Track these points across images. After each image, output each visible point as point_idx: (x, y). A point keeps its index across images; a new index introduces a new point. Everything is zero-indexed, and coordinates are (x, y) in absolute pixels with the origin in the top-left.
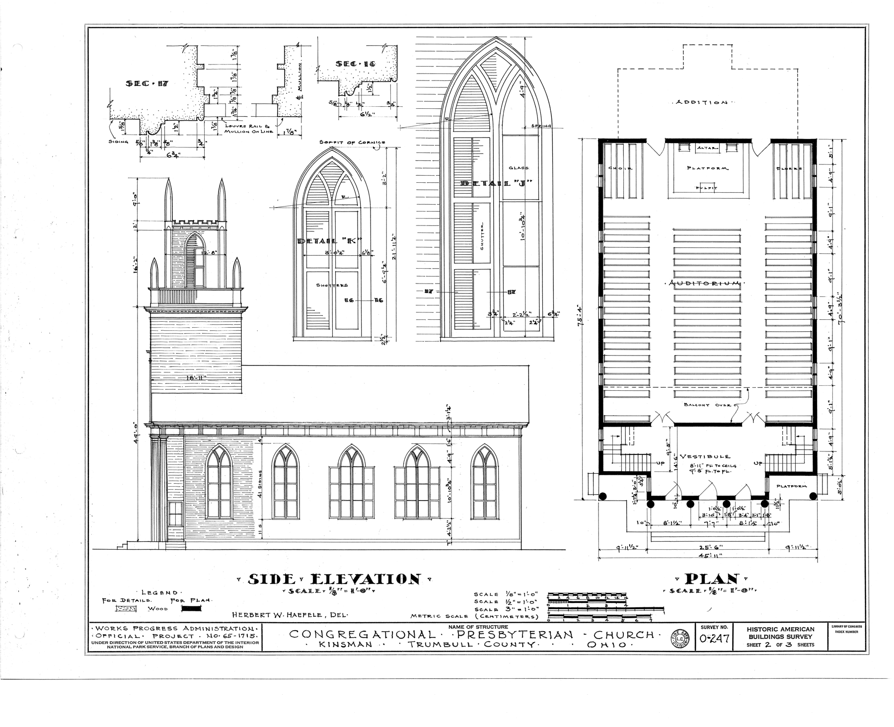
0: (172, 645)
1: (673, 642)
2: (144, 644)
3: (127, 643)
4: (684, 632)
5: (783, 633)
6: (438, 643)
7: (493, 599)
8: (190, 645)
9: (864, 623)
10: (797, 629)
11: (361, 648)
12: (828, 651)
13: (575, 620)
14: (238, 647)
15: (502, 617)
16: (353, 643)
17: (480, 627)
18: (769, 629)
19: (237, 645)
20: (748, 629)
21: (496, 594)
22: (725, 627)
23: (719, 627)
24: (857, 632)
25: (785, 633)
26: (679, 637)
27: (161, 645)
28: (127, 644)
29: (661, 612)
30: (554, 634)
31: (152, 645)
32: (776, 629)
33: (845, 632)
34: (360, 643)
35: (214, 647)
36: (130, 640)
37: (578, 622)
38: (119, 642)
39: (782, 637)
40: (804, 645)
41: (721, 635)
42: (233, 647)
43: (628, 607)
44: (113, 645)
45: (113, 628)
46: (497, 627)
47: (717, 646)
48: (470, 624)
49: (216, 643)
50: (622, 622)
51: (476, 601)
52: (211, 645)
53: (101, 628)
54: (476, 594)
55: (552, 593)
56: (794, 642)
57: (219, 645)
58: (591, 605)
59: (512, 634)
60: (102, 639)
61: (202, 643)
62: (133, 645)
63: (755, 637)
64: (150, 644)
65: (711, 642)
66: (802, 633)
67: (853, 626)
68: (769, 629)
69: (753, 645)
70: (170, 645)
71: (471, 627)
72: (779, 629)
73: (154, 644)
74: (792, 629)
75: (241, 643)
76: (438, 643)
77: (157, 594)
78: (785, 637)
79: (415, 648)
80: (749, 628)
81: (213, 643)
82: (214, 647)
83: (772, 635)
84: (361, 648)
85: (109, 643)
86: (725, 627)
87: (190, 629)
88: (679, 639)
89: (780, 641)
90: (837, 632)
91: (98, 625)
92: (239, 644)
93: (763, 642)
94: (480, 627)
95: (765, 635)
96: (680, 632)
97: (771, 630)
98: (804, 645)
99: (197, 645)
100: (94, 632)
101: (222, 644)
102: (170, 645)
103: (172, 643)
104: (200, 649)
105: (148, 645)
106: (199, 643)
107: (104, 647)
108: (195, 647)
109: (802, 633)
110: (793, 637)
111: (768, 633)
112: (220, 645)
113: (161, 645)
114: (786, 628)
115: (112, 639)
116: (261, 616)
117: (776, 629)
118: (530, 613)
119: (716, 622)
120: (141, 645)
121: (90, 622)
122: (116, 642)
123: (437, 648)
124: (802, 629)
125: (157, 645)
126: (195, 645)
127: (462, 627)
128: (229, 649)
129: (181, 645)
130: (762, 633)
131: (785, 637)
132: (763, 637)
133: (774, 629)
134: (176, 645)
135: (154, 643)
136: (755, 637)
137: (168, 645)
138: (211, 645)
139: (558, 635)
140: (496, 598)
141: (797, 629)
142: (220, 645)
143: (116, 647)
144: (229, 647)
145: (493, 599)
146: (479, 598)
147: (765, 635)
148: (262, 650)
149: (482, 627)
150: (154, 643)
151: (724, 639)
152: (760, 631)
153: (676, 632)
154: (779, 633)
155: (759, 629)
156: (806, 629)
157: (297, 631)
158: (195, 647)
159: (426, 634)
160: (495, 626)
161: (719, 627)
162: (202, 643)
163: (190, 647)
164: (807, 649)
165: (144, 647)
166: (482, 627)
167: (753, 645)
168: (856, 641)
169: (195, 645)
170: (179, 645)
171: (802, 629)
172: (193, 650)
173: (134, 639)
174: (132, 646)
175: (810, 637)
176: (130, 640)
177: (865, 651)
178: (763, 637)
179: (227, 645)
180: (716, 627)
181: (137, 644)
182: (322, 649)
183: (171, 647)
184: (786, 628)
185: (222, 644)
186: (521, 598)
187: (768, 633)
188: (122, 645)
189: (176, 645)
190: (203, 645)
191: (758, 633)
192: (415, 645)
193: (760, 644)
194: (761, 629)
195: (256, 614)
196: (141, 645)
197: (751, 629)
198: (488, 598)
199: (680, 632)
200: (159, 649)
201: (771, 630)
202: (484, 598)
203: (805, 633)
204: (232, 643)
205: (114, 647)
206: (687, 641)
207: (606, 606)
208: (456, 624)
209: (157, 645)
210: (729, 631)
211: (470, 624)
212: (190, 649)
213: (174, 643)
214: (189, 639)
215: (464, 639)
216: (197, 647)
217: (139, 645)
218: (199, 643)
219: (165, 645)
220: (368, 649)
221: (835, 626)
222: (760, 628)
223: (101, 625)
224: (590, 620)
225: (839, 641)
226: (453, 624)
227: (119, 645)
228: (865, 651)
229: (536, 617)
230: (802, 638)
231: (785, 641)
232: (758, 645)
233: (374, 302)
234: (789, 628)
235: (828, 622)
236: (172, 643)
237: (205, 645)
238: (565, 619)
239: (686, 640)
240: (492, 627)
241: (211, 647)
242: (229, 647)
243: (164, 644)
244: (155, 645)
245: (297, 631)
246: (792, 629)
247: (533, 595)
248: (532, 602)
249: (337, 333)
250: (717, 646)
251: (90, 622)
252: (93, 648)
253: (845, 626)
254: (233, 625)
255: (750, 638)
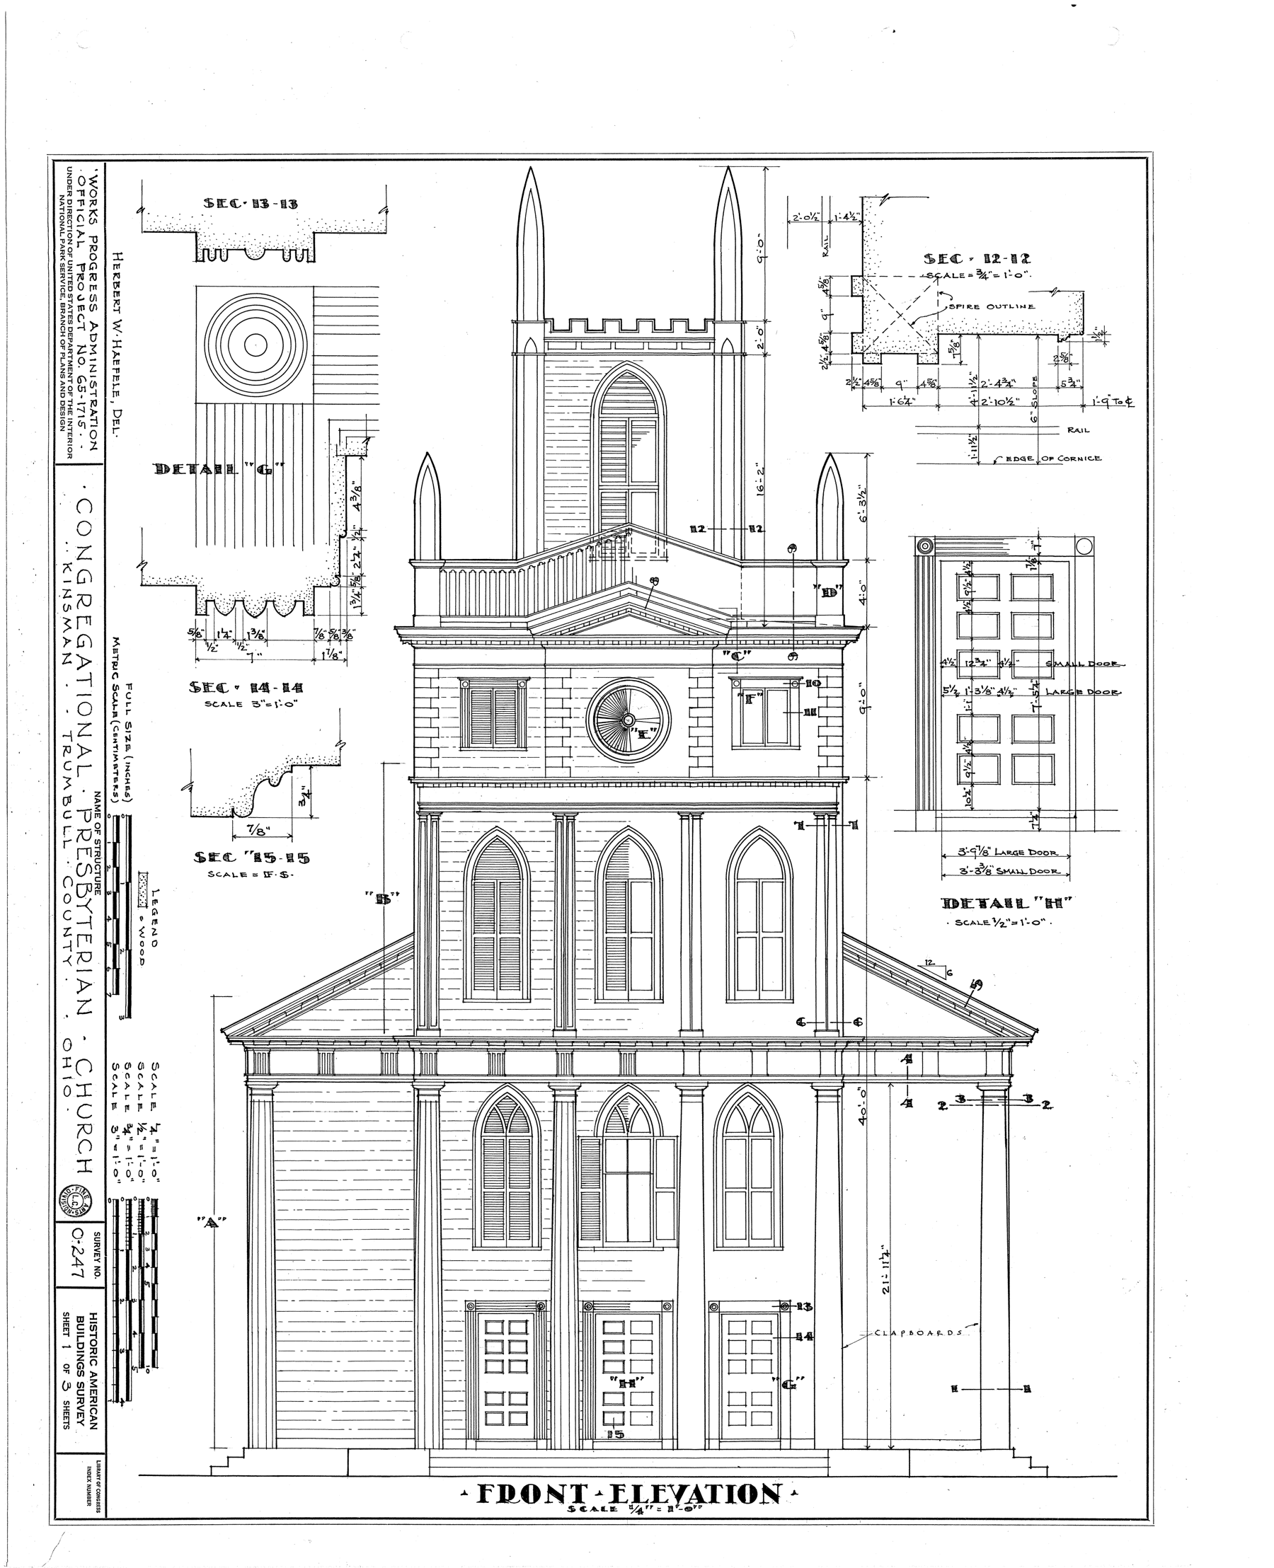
0: (67, 307)
1: (70, 1188)
2: (67, 258)
3: (70, 229)
4: (87, 1208)
5: (87, 1374)
6: (70, 785)
7: (146, 1101)
8: (66, 338)
9: (104, 1517)
10: (94, 1400)
11: (60, 642)
12: (56, 1453)
13: (110, 913)
14: (62, 423)
15: (116, 753)
16: (70, 628)
17: (98, 846)
18: (94, 1350)
19: (66, 420)
20: (93, 1314)
21: (154, 1104)
22: (97, 1274)
23: (97, 1264)
24: (89, 1504)
25: (86, 1380)
26: (79, 1199)
27: (66, 288)
28: (66, 229)
29: (123, 1012)
30: (85, 977)
31: (66, 272)
32: (94, 1363)
33: (89, 1483)
34: (70, 641)
35: (63, 380)
36: (75, 234)
37: (106, 969)
38: (70, 216)
39: (81, 1373)
40: (67, 1412)
41: (83, 1264)
42: (62, 414)
43: (133, 1336)
44: (66, 205)
45: (94, 202)
46: (98, 875)
47: (65, 1258)
48: (102, 829)
49: (70, 384)
50: (106, 944)
51: (141, 1066)
52: (67, 375)
53: (94, 184)
54: (155, 1066)
55: (156, 1215)
56: (72, 1396)
57: (66, 389)
58: (135, 1275)
59: (86, 906)
60: (76, 186)
61: (70, 359)
62: (66, 239)
63: (80, 1327)
64: (67, 269)
65: (73, 1247)
66: (87, 1408)
67: (98, 1496)
68: (94, 1350)
69: (66, 1323)
70: (67, 303)
71: (98, 831)
72: (94, 1369)
73: (67, 276)
74: (94, 1390)
75: (70, 427)
76: (70, 785)
77: (154, 914)
78: (81, 1379)
79: (61, 742)
80: (95, 1316)
81: (70, 379)
82: (63, 380)
83: (83, 1356)
84: (60, 642)
85: (69, 198)
86: (97, 1274)
87: (93, 332)
88: (76, 1199)
89: (73, 1369)
90: (89, 1468)
91: (100, 180)
92: (67, 424)
93: (72, 1340)
94: (98, 846)
95: (83, 1343)
96: (87, 1201)
97: (93, 1355)
98: (67, 1412)
99: (66, 351)
100: (88, 170)
101: (67, 395)
102: (67, 303)
103: (71, 307)
104: (59, 356)
105: (67, 265)
106: (70, 355)
107: (61, 189)
108: (63, 347)
109: (87, 1408)
110: (80, 1393)
111: (87, 1350)
112: (67, 391)
113: (66, 288)
114: (96, 1380)
115: (76, 205)
116: (116, 301)
117: (94, 1363)
118: (119, 1099)
119: (106, 1258)
120: (66, 252)
121: (105, 164)
122: (70, 211)
123: (61, 783)
124: (94, 1407)
125: (67, 280)
126: (67, 348)
127: (98, 815)
128: (58, 406)
129: (66, 323)
130: (86, 1339)
131: (81, 1379)
132: (81, 1340)
133: (94, 1360)
134: (66, 314)
135: (70, 276)
136: (80, 1327)
137: (65, 300)
138: (67, 375)
139: (84, 985)
140: (147, 1106)
141: (94, 1400)
142: (67, 391)
143: (62, 211)
144: (63, 407)
145: (146, 1101)
146: (147, 1071)
147: (83, 1343)
148: (57, 464)
149: (98, 850)
150: (70, 276)
151: (78, 1270)
152: (91, 1335)
153: (87, 1194)
154: (87, 1369)
155: (94, 1333)
156: (94, 1415)
157: (77, 1085)
158: (63, 347)
159: (84, 760)
160: (100, 873)
161: (97, 1264)
162: (70, 359)
163: (63, 338)
164: (59, 1417)
165: (63, 258)
166: (98, 850)
167: (66, 1323)
168: (73, 1501)
169: (67, 348)
170: (66, 319)
171: (94, 1407)
172: (58, 344)
173: (75, 240)
174: (65, 236)
175: (81, 1422)
176: (75, 234)
177: (56, 1519)
178: (81, 1340)
179: (67, 403)
180: (97, 1258)
181: (67, 246)
182: (60, 568)
183: (63, 304)
184: (96, 1380)
185: (67, 395)
186: (147, 1152)
187: (87, 1350)
188: (66, 220)
189: (66, 314)
190: (65, 361)
191: (87, 1332)
192: (67, 741)
193: (68, 1334)
194: (94, 1337)
195: (118, 292)
196: (66, 252)
197: (94, 1319)
198: (147, 1090)
199: (87, 1201)
200: (58, 211)
201: (93, 1355)
202: (147, 1081)
203: (87, 1414)
204: (70, 412)
205: (62, 207)
206: (71, 1214)
207: (134, 1268)
208: (102, 803)
209: (66, 281)
210: (90, 1280)
211: (102, 829)
212: (59, 339)
213: (70, 310)
214: (75, 324)
215: (78, 821)
216: (63, 351)
217: (66, 249)
218: (70, 355)
219: (66, 295)
220: (60, 659)
221: (99, 1466)
222: (96, 1335)
223: (100, 184)
224: (109, 940)
225: (73, 1473)
226: (102, 798)
227: (66, 215)
228: (56, 1519)
229: (115, 799)
230: (78, 1408)
231: (73, 1378)
232: (66, 1332)
233: (708, 524)
234: (96, 1386)
235: (106, 1454)
236: (71, 307)
237: (67, 364)
238: (112, 844)
239: (74, 1211)
240: (98, 867)
241: (62, 376)
242: (63, 407)
243: (67, 293)
244: (66, 278)
245: (77, 1085)
246: (94, 1390)
247: (154, 1173)
248: (141, 1174)
249: (753, 1243)
250: (65, 1258)
251: (105, 164)
252: (61, 168)
253: (98, 1484)
254: (100, 415)
255: (78, 1317)
